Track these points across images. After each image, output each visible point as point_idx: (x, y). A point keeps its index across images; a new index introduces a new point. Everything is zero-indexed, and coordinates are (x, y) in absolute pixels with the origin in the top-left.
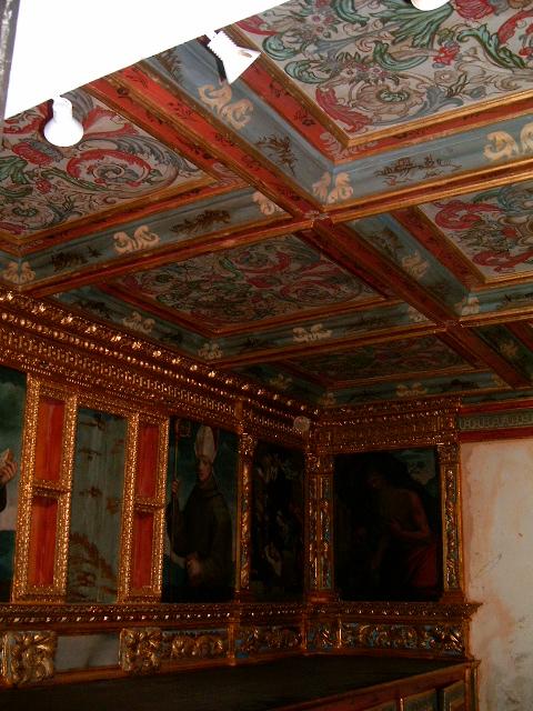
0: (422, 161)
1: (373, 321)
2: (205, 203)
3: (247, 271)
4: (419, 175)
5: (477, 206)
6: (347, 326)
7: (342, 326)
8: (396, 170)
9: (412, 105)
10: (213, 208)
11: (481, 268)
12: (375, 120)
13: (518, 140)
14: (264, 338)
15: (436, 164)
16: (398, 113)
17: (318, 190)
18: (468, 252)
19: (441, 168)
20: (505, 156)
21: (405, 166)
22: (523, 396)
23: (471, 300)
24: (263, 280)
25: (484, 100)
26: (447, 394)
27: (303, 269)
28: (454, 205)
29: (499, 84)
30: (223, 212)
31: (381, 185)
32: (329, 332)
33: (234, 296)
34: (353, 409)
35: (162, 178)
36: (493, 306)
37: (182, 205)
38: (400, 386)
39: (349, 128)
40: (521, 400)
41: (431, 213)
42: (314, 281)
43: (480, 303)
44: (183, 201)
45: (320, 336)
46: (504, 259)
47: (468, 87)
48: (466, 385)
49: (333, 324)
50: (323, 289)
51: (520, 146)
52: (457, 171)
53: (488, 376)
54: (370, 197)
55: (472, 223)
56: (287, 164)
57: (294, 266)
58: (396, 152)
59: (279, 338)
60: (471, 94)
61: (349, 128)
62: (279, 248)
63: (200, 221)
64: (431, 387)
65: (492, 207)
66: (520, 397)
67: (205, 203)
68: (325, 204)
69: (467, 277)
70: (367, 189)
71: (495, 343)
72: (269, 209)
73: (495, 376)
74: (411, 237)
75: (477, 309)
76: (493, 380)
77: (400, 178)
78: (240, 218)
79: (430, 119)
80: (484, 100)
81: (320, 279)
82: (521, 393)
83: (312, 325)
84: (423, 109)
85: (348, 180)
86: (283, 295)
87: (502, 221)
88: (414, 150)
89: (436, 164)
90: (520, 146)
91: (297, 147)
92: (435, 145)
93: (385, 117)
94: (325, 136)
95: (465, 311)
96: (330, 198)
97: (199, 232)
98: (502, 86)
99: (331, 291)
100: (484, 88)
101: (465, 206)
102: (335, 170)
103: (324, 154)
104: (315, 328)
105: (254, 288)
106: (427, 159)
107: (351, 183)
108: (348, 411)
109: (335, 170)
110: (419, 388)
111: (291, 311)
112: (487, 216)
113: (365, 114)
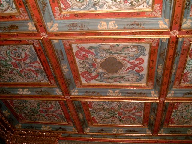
0: (80, 25)
1: (44, 91)
2: (12, 22)
3: (14, 58)
4: (78, 29)
5: (88, 51)
6: (35, 91)
7: (34, 91)
8: (72, 26)
9: (83, 5)
10: (14, 24)
11: (82, 78)
12: (71, 7)
13: (108, 25)
14: (8, 90)
15: (84, 27)
16: (79, 7)
17: (48, 25)
18: (80, 70)
19: (85, 28)
20: (103, 29)
21: (75, 25)
22: (80, 137)
23: (76, 91)
24: (16, 64)
25: (103, 10)
26: (57, 131)
27: (30, 63)
28: (82, 49)
29: (108, 5)
30: (17, 26)
31: (67, 29)
32: (30, 92)
33: (5, 69)
34: (26, 131)
35: (3, 8)
36: (82, 94)
37: (4, 21)
38: (43, 126)
39: (64, 7)
40: (80, 138)
41: (75, 49)
42: (32, 70)
43: (78, 92)
44: (5, 20)
45: (26, 93)
46: (89, 77)
47: (100, 4)
48: (64, 129)
49: (32, 90)
50: (33, 74)
51: (108, 26)
52: (89, 30)
53: (71, 128)
54: (62, 32)
55: (85, 57)
56: (43, 12)
57: (28, 61)
58: (74, 21)
59: (12, 91)
60: (99, 6)
61: (64, 7)
62: (26, 52)
63: (8, 28)
64: (52, 128)
65: (92, 53)
66: (79, 137)
67: (12, 22)
68: (49, 31)
69: (77, 82)
70: (62, 29)
71: (78, 111)
72: (31, 27)
73: (73, 128)
74: (66, 58)
75: (77, 94)
76: (72, 129)
77: (72, 28)
78: (22, 29)
79: (86, 12)
80: (103, 10)
81: (34, 69)
82: (80, 136)
83: (25, 89)
84: (85, 7)
85: (58, 25)
86: (20, 73)
87: (93, 59)
88: (79, 21)
89: (84, 27)
90: (108, 26)
91: (48, 8)
92: (85, 21)
93: (75, 7)
94: (56, 8)
95: (73, 94)
96: (50, 30)
97: (7, 31)
98: (108, 6)
99: (35, 76)
100: (104, 5)
101: (85, 50)
102: (55, 22)
103: (54, 15)
104: (25, 90)
105: (12, 67)
106: (82, 24)
107: (58, 27)
108: (24, 132)
109: (55, 22)
110: (50, 128)
111: (20, 82)
112: (91, 56)
113: (70, 4)
